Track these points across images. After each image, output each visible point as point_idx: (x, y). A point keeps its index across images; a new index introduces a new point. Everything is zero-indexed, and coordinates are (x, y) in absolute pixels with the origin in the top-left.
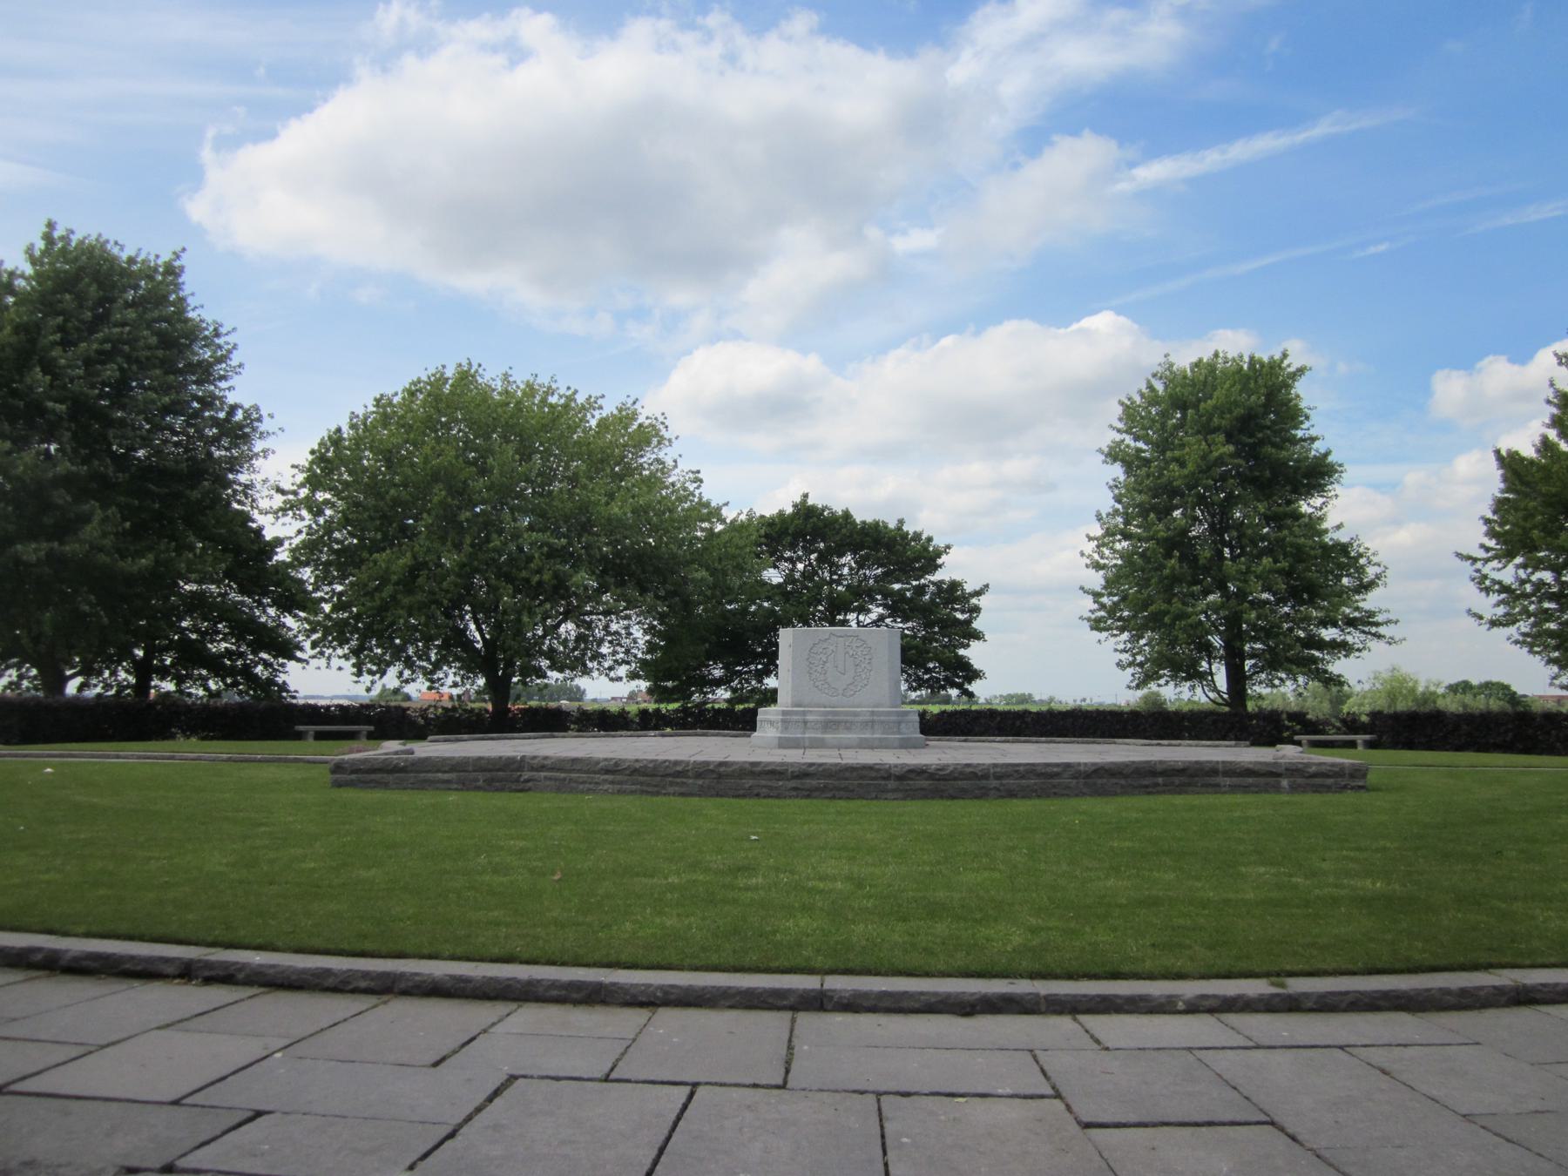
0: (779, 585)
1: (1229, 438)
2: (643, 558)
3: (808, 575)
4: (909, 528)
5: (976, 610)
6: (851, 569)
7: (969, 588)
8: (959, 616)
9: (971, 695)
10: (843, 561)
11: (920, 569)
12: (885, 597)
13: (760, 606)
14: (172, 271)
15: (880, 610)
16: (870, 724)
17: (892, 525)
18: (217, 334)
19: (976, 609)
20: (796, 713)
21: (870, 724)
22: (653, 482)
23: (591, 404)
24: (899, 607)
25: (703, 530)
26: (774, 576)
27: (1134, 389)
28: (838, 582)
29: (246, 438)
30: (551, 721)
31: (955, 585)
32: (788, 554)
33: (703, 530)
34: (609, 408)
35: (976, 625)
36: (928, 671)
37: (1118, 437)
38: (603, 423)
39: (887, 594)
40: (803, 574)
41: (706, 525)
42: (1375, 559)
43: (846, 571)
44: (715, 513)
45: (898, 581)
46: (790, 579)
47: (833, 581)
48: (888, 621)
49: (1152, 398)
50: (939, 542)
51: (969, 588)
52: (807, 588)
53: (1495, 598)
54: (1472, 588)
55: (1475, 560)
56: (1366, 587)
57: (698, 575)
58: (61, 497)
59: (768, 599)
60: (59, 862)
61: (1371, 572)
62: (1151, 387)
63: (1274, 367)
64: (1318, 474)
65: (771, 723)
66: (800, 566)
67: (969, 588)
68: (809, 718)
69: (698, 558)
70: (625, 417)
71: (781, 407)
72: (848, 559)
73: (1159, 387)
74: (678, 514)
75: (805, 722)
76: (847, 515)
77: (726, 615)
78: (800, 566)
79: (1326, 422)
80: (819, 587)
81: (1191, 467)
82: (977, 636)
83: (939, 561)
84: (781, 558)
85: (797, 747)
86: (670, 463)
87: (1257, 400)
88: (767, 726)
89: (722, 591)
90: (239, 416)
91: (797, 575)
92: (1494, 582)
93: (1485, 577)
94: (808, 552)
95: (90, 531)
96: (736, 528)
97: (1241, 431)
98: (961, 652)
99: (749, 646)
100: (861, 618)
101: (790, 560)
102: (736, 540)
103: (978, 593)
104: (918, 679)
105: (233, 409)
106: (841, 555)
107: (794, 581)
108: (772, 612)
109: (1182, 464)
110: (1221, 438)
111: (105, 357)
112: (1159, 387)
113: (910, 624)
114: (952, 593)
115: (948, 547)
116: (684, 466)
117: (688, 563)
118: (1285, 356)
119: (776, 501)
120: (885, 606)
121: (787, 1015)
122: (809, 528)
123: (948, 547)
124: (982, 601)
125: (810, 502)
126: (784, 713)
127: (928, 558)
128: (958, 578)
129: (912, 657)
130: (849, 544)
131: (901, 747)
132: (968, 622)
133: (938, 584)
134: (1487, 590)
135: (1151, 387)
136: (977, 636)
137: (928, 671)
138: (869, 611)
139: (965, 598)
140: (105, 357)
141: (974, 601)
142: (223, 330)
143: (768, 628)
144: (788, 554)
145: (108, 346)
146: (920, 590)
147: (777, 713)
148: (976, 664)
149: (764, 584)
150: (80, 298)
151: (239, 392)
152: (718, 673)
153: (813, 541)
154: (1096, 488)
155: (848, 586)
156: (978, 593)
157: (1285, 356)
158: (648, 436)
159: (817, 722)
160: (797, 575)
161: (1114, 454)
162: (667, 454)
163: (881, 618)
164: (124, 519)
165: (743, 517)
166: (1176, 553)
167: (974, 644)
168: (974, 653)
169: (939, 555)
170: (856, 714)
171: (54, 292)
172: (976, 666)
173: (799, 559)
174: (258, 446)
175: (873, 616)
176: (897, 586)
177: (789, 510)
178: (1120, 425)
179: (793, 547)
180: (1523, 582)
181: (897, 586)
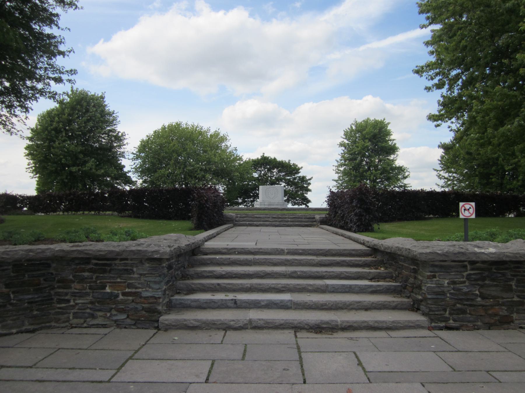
1: (370, 140)
2: (223, 170)
3: (265, 175)
4: (292, 162)
5: (310, 184)
7: (307, 178)
8: (305, 185)
9: (308, 206)
10: (274, 171)
14: (102, 97)
17: (287, 161)
18: (113, 113)
19: (310, 184)
22: (224, 151)
23: (209, 130)
26: (256, 175)
27: (347, 127)
28: (273, 177)
29: (121, 140)
30: (192, 277)
31: (304, 177)
32: (260, 169)
34: (212, 131)
35: (309, 188)
36: (297, 200)
37: (343, 140)
38: (211, 135)
39: (285, 180)
40: (263, 174)
41: (238, 162)
42: (408, 170)
43: (275, 173)
44: (240, 159)
45: (288, 176)
46: (260, 176)
47: (271, 176)
49: (352, 130)
53: (443, 181)
54: (437, 178)
55: (437, 171)
56: (405, 178)
57: (236, 174)
58: (81, 156)
60: (263, 172)
61: (407, 174)
62: (351, 127)
63: (382, 122)
64: (393, 150)
66: (263, 172)
67: (307, 178)
69: (237, 170)
70: (216, 134)
71: (265, 121)
72: (275, 170)
73: (354, 128)
74: (231, 159)
76: (275, 159)
77: (243, 185)
79: (396, 136)
80: (267, 178)
81: (359, 148)
82: (310, 190)
86: (229, 145)
87: (376, 131)
89: (242, 179)
90: (120, 134)
92: (443, 176)
93: (440, 175)
94: (265, 168)
95: (89, 165)
96: (246, 162)
97: (373, 138)
98: (305, 195)
101: (260, 171)
102: (246, 166)
103: (310, 179)
105: (119, 132)
106: (274, 169)
107: (261, 176)
108: (255, 184)
109: (358, 147)
110: (367, 141)
111: (88, 121)
112: (354, 128)
114: (303, 179)
116: (233, 146)
117: (235, 171)
118: (384, 119)
119: (256, 156)
120: (286, 183)
121: (302, 354)
122: (264, 162)
124: (311, 182)
125: (265, 156)
132: (307, 187)
133: (299, 177)
134: (441, 178)
135: (351, 127)
136: (310, 190)
137: (297, 200)
139: (307, 181)
140: (88, 121)
141: (309, 181)
142: (115, 112)
143: (256, 188)
145: (89, 118)
146: (295, 179)
149: (253, 177)
150: (82, 106)
151: (120, 128)
152: (240, 201)
153: (266, 166)
154: (336, 154)
156: (310, 179)
157: (384, 119)
158: (223, 139)
161: (342, 145)
162: (228, 144)
165: (248, 160)
167: (309, 193)
168: (309, 195)
171: (76, 105)
172: (309, 199)
173: (263, 170)
174: (125, 142)
176: (288, 178)
177: (260, 158)
178: (344, 137)
180: (450, 177)
181: (288, 178)
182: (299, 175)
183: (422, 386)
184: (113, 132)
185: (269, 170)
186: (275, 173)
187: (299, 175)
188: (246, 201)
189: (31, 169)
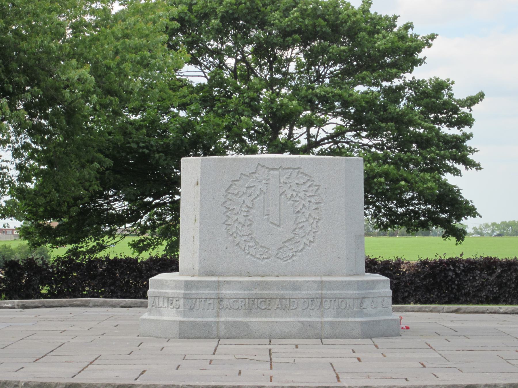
0: (201, 88)
3: (244, 74)
6: (299, 65)
10: (288, 54)
11: (393, 65)
12: (346, 104)
13: (175, 116)
15: (339, 120)
16: (319, 301)
20: (208, 285)
21: (319, 301)
24: (366, 117)
25: (93, 12)
26: (194, 75)
28: (282, 83)
32: (213, 44)
33: (93, 12)
36: (401, 203)
40: (234, 71)
43: (292, 67)
45: (363, 81)
46: (216, 80)
48: (349, 135)
50: (420, 31)
51: (459, 92)
52: (237, 89)
59: (183, 106)
65: (169, 299)
68: (225, 292)
69: (78, 53)
75: (220, 299)
78: (230, 62)
83: (420, 56)
84: (204, 51)
85: (208, 337)
88: (162, 303)
89: (110, 89)
91: (227, 75)
94: (243, 38)
98: (449, 178)
99: (146, 172)
100: (313, 131)
103: (472, 101)
104: (390, 212)
107: (221, 83)
113: (377, 141)
114: (434, 98)
115: (433, 37)
120: (345, 115)
123: (433, 37)
126: (188, 285)
127: (407, 52)
128: (443, 77)
129: (380, 189)
130: (299, 31)
131: (365, 335)
133: (414, 85)
138: (322, 123)
144: (213, 44)
146: (394, 94)
147: (177, 284)
148: (466, 195)
152: (120, 206)
155: (296, 89)
156: (472, 101)
159: (237, 299)
160: (227, 75)
163: (340, 132)
164: (350, 121)
166: (284, 133)
168: (464, 182)
169: (419, 49)
170: (295, 286)
173: (230, 52)
175: (330, 129)
179: (220, 34)
181: (361, 89)
182: (419, 74)
183: (177, 366)
184: (53, 201)
185: (263, 50)
186: (292, 67)
187: (419, 74)
188: (148, 207)
189: (295, 137)
